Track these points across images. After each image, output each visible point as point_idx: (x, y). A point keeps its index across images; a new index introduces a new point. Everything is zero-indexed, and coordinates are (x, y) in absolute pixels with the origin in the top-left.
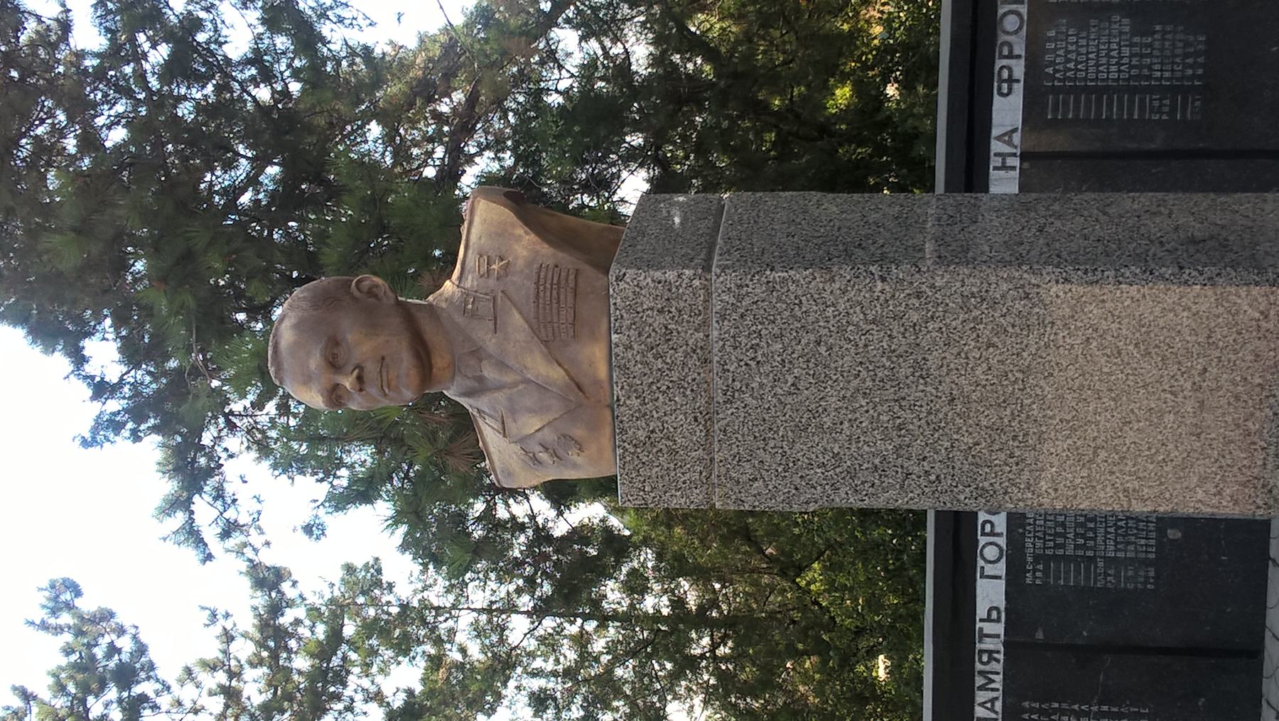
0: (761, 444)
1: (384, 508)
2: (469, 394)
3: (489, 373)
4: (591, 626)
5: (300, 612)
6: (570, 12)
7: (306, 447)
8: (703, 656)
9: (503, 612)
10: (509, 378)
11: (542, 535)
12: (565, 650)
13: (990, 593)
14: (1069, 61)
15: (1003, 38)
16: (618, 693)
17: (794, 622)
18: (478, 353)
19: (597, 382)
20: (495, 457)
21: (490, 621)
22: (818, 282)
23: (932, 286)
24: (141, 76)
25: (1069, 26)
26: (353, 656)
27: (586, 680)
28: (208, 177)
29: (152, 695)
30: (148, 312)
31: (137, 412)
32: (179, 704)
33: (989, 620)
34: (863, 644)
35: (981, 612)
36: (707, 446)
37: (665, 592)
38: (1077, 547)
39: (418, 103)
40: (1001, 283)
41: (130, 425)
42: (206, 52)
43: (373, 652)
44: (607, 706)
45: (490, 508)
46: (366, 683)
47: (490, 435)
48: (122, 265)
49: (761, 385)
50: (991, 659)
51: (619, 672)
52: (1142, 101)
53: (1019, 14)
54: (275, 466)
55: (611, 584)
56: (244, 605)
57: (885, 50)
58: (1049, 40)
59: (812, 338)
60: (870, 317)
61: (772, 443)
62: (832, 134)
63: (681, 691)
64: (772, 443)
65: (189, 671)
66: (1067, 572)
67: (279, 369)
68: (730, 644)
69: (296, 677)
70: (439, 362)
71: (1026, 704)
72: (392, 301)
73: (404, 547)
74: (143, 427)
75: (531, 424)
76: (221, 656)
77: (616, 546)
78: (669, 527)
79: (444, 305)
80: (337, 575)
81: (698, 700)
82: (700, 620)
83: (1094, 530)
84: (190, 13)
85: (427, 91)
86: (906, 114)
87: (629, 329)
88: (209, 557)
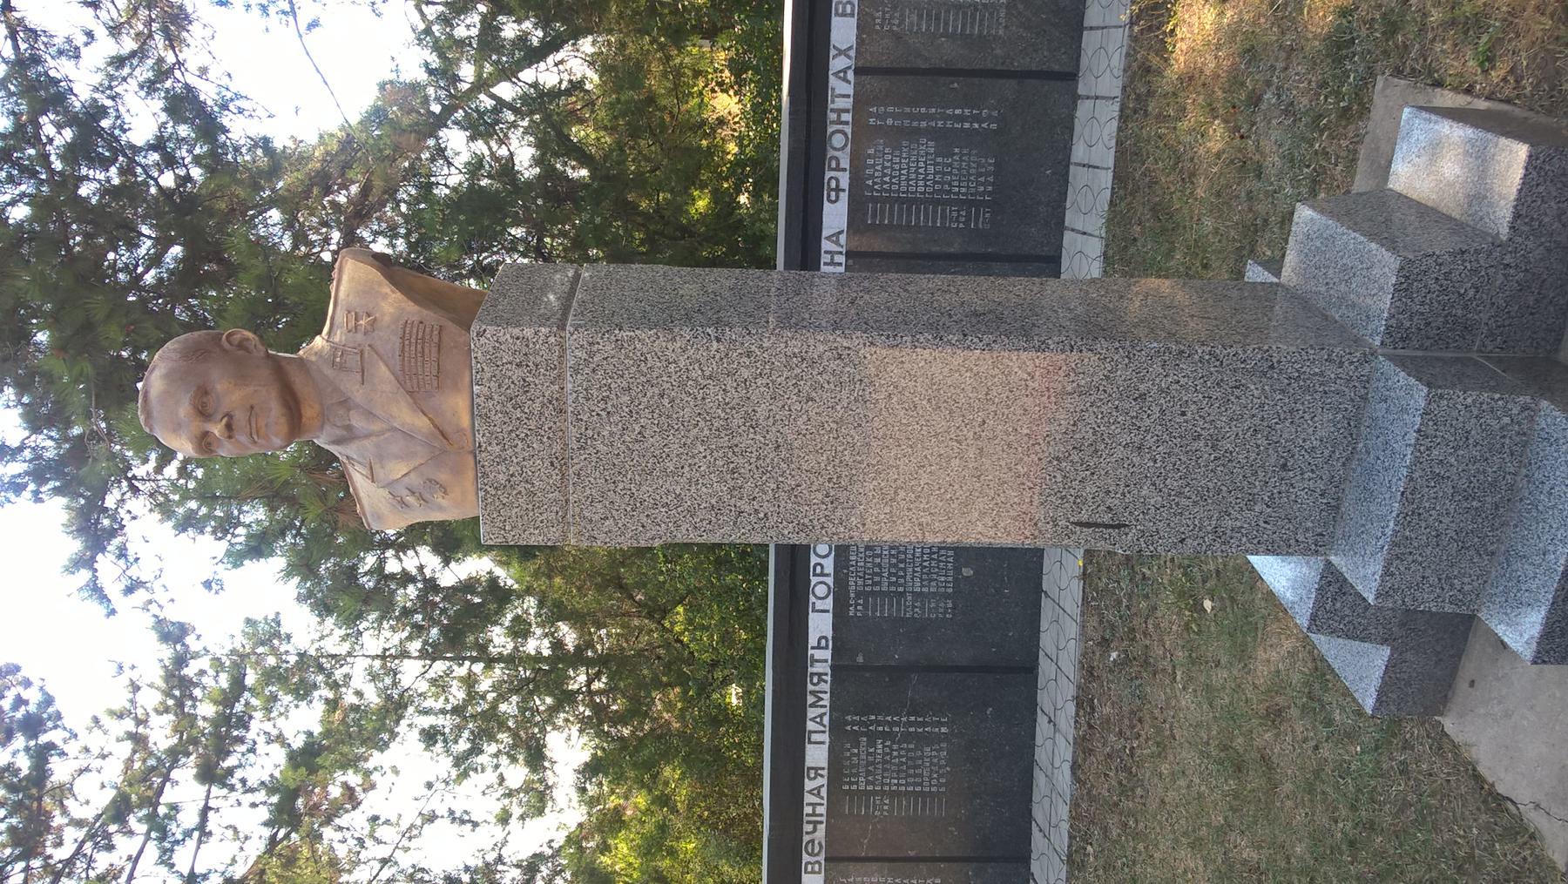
0: (612, 487)
1: (278, 562)
2: (338, 442)
3: (358, 422)
4: (478, 668)
5: (204, 663)
6: (460, 114)
7: (206, 503)
8: (578, 691)
9: (395, 657)
10: (376, 427)
11: (431, 585)
12: (454, 690)
13: (820, 625)
14: (885, 175)
15: (831, 153)
16: (502, 726)
17: (659, 658)
18: (346, 403)
19: (460, 431)
20: (365, 502)
21: (383, 666)
22: (661, 342)
23: (761, 347)
24: (45, 157)
25: (885, 145)
26: (254, 702)
27: (472, 716)
28: (111, 256)
29: (59, 743)
30: (49, 379)
31: (40, 472)
32: (87, 750)
33: (819, 647)
34: (719, 674)
35: (812, 641)
36: (562, 487)
37: (546, 635)
38: (890, 584)
39: (315, 191)
40: (818, 345)
41: (32, 486)
42: (111, 139)
43: (274, 698)
44: (492, 738)
45: (382, 562)
46: (268, 727)
47: (360, 481)
48: (27, 337)
49: (612, 434)
50: (820, 680)
51: (503, 707)
52: (943, 211)
53: (845, 134)
54: (175, 527)
55: (497, 630)
56: (152, 659)
57: (738, 163)
58: (869, 156)
59: (656, 391)
60: (707, 373)
61: (621, 486)
62: (692, 235)
63: (560, 722)
64: (621, 486)
65: (96, 720)
66: (882, 606)
67: (148, 416)
68: (604, 680)
69: (201, 723)
70: (309, 412)
71: (849, 718)
72: (262, 354)
73: (300, 599)
74: (43, 489)
75: (398, 469)
76: (128, 705)
77: (498, 595)
78: (550, 577)
79: (313, 358)
80: (239, 626)
81: (575, 729)
82: (577, 658)
83: (904, 569)
84: (95, 100)
85: (324, 182)
86: (755, 218)
87: (490, 380)
88: (113, 612)
